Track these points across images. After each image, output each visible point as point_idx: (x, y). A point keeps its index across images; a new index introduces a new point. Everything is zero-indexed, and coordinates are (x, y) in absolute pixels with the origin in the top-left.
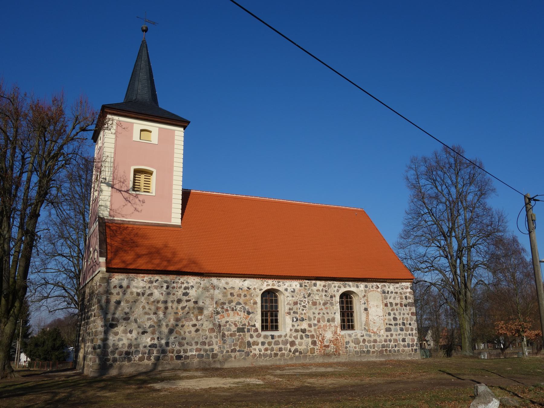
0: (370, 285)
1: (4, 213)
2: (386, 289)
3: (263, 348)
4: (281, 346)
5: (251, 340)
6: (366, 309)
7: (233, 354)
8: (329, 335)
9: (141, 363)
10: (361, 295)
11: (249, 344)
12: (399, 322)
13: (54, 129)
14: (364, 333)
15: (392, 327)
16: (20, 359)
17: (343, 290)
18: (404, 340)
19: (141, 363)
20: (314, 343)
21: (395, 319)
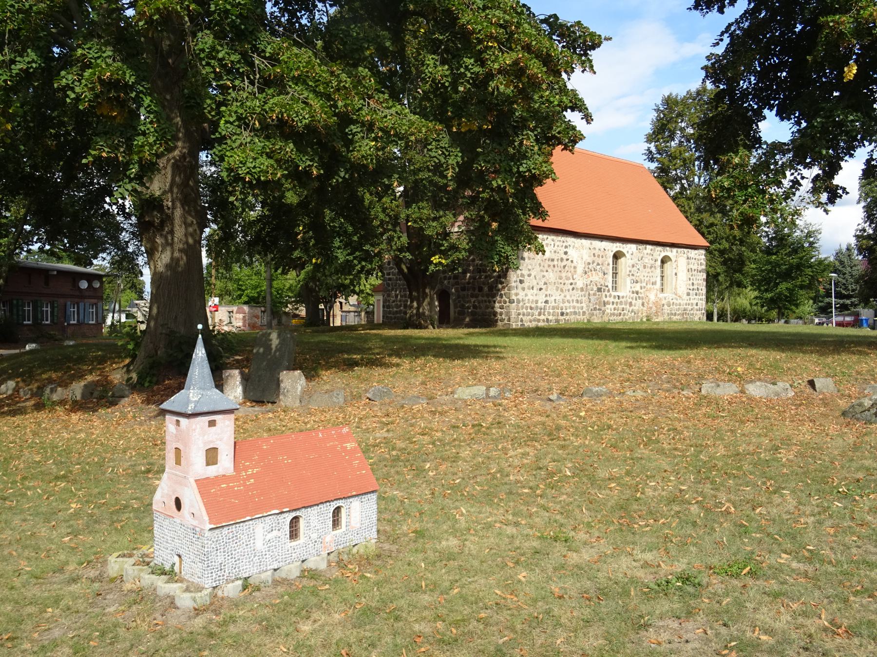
0: (679, 250)
1: (205, 261)
2: (690, 255)
3: (613, 307)
4: (623, 306)
5: (606, 300)
6: (676, 274)
7: (595, 312)
8: (652, 297)
9: (294, 514)
10: (673, 259)
11: (605, 304)
12: (695, 287)
13: (44, 244)
14: (674, 296)
15: (691, 292)
16: (356, 364)
17: (663, 254)
18: (697, 305)
19: (294, 514)
20: (643, 305)
21: (693, 284)
